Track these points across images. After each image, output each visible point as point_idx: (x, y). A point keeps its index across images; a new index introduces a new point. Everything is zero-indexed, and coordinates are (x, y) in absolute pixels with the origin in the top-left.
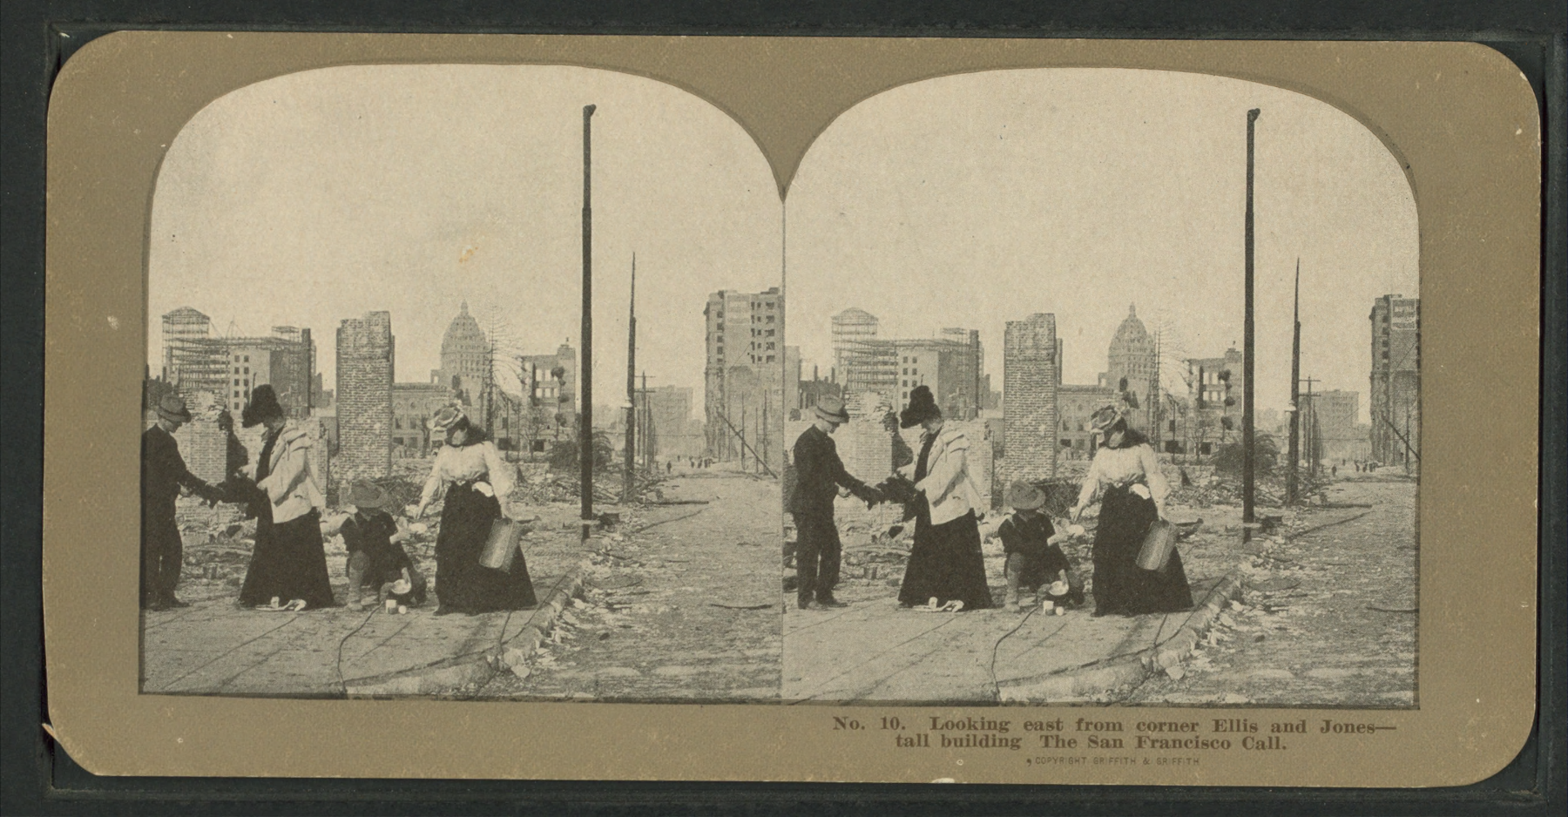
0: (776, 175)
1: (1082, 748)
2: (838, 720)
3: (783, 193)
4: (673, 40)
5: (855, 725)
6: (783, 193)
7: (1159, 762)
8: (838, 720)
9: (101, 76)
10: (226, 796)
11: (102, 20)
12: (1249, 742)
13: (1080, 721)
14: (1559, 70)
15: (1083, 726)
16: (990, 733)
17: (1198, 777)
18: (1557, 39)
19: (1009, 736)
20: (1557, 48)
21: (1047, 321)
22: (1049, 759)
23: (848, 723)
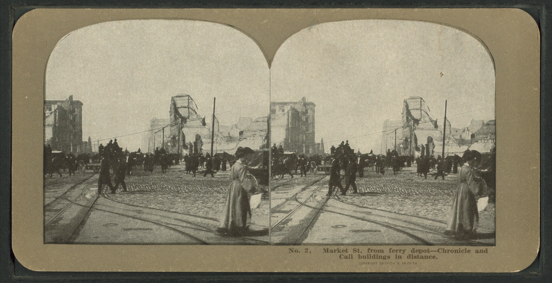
0: (266, 56)
1: (393, 259)
2: (290, 249)
3: (270, 63)
4: (191, 9)
5: (297, 251)
6: (270, 63)
7: (381, 264)
8: (290, 249)
9: (29, 25)
10: (76, 278)
11: (29, 5)
12: (342, 257)
13: (369, 249)
14: (544, 18)
15: (370, 251)
16: (376, 254)
17: (390, 269)
18: (544, 7)
19: (347, 254)
20: (544, 10)
21: (79, 104)
22: (364, 263)
23: (294, 250)
